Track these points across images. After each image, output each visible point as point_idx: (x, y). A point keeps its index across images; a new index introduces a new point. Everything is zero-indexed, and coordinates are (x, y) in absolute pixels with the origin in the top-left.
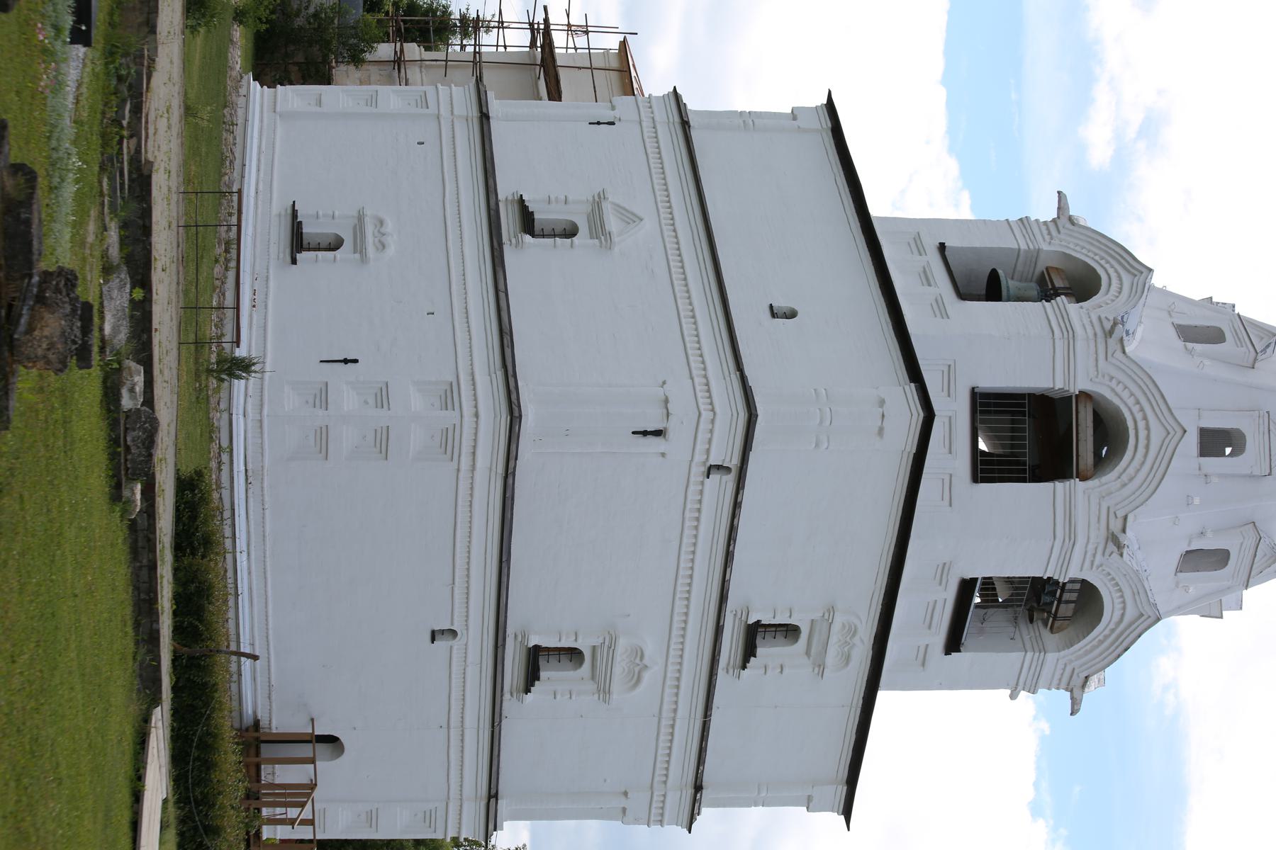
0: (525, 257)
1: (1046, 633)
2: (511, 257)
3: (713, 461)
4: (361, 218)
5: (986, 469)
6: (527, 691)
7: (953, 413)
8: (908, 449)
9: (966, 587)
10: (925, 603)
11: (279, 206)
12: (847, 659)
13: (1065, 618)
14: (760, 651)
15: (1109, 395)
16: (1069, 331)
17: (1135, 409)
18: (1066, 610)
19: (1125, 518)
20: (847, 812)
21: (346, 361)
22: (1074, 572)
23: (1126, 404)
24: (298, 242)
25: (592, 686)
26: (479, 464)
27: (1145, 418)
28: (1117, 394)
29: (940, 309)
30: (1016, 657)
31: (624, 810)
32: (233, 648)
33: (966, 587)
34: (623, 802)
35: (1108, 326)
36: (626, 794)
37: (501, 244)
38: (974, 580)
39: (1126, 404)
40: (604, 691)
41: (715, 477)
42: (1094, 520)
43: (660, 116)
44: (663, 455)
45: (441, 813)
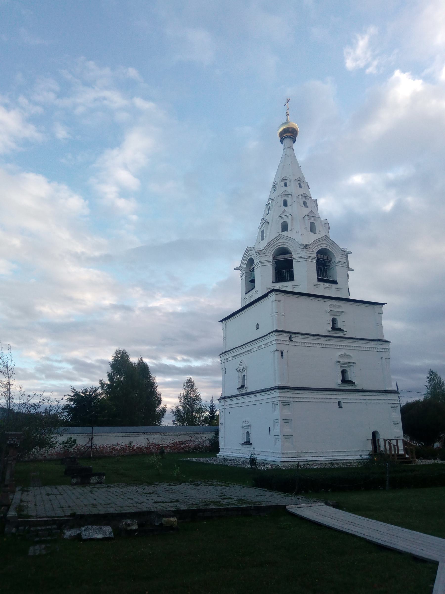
0: (250, 387)
1: (332, 262)
2: (249, 391)
3: (289, 340)
4: (243, 427)
5: (291, 278)
6: (354, 383)
7: (277, 286)
9: (319, 280)
10: (323, 289)
11: (240, 447)
12: (339, 306)
13: (328, 258)
14: (339, 327)
15: (273, 252)
16: (261, 262)
17: (276, 246)
18: (325, 257)
20: (383, 304)
21: (270, 431)
22: (315, 256)
24: (247, 443)
25: (352, 367)
26: (292, 396)
29: (256, 292)
30: (338, 268)
31: (386, 358)
32: (296, 468)
33: (319, 280)
34: (384, 359)
35: (258, 254)
36: (382, 358)
37: (247, 393)
38: (318, 278)
40: (353, 364)
41: (293, 339)
42: (302, 252)
43: (223, 358)
44: (287, 351)
45: (392, 405)
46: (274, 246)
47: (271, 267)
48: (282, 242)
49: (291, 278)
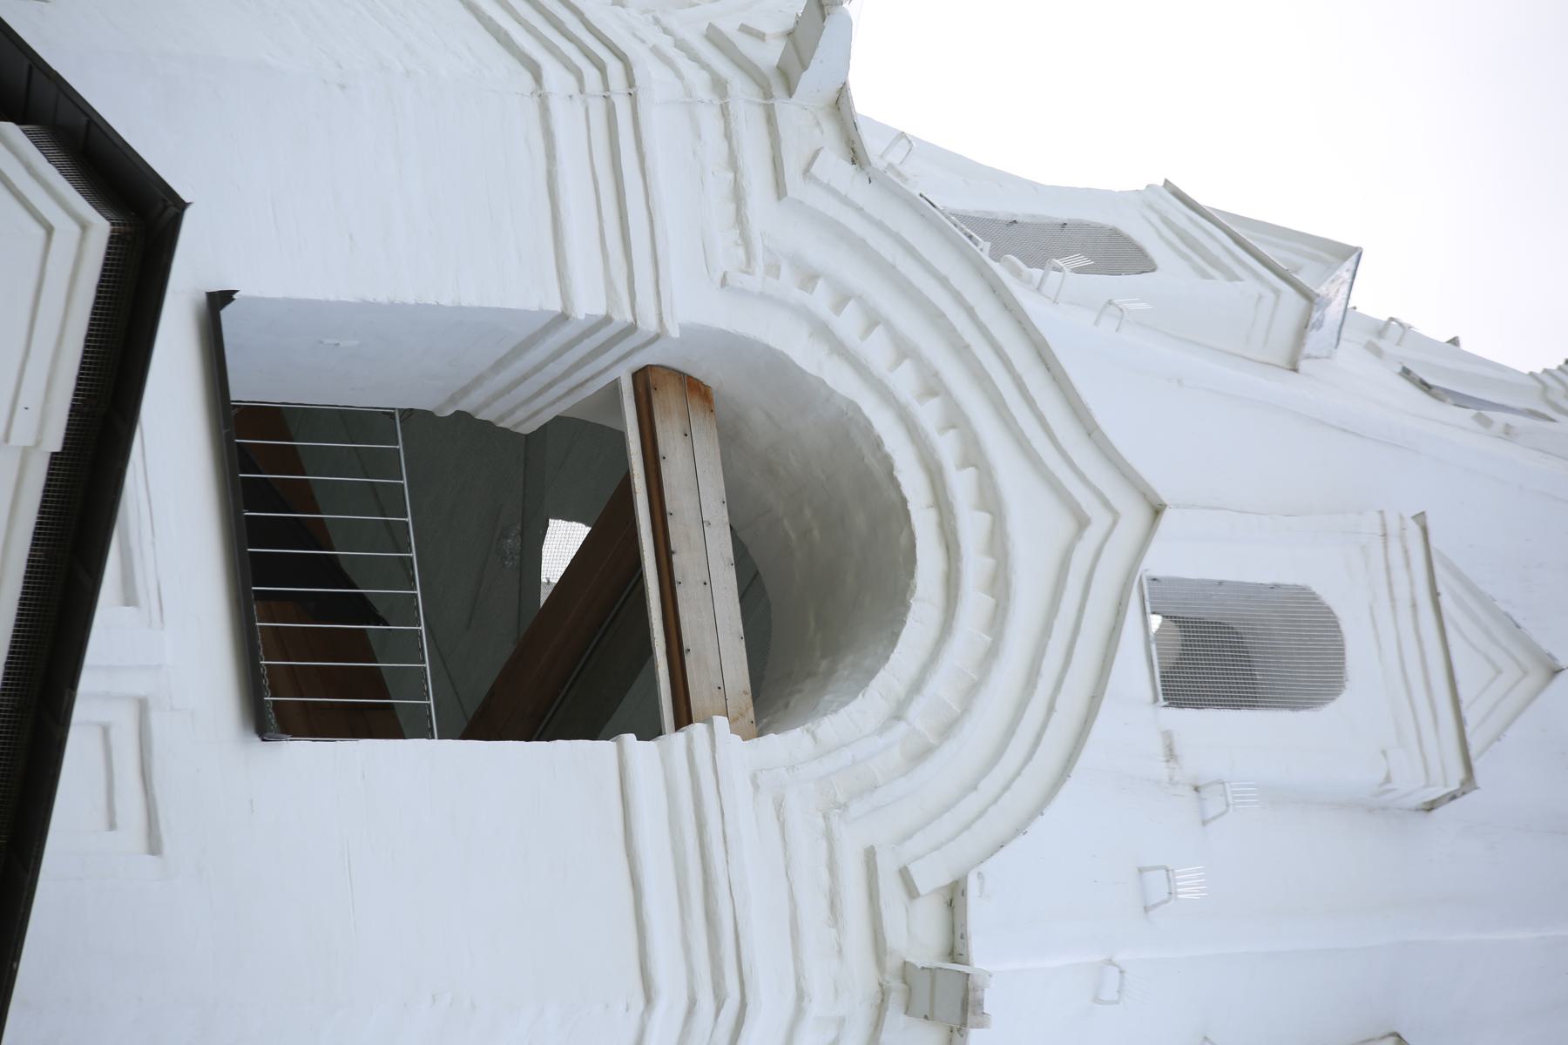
5: (316, 662)
8: (23, 434)
15: (807, 355)
17: (928, 414)
19: (954, 898)
23: (886, 395)
27: (974, 455)
28: (840, 350)
35: (769, 54)
38: (678, 726)
39: (886, 395)
42: (813, 910)
46: (933, 386)
47: (525, 291)
48: (998, 544)
49: (316, 662)
